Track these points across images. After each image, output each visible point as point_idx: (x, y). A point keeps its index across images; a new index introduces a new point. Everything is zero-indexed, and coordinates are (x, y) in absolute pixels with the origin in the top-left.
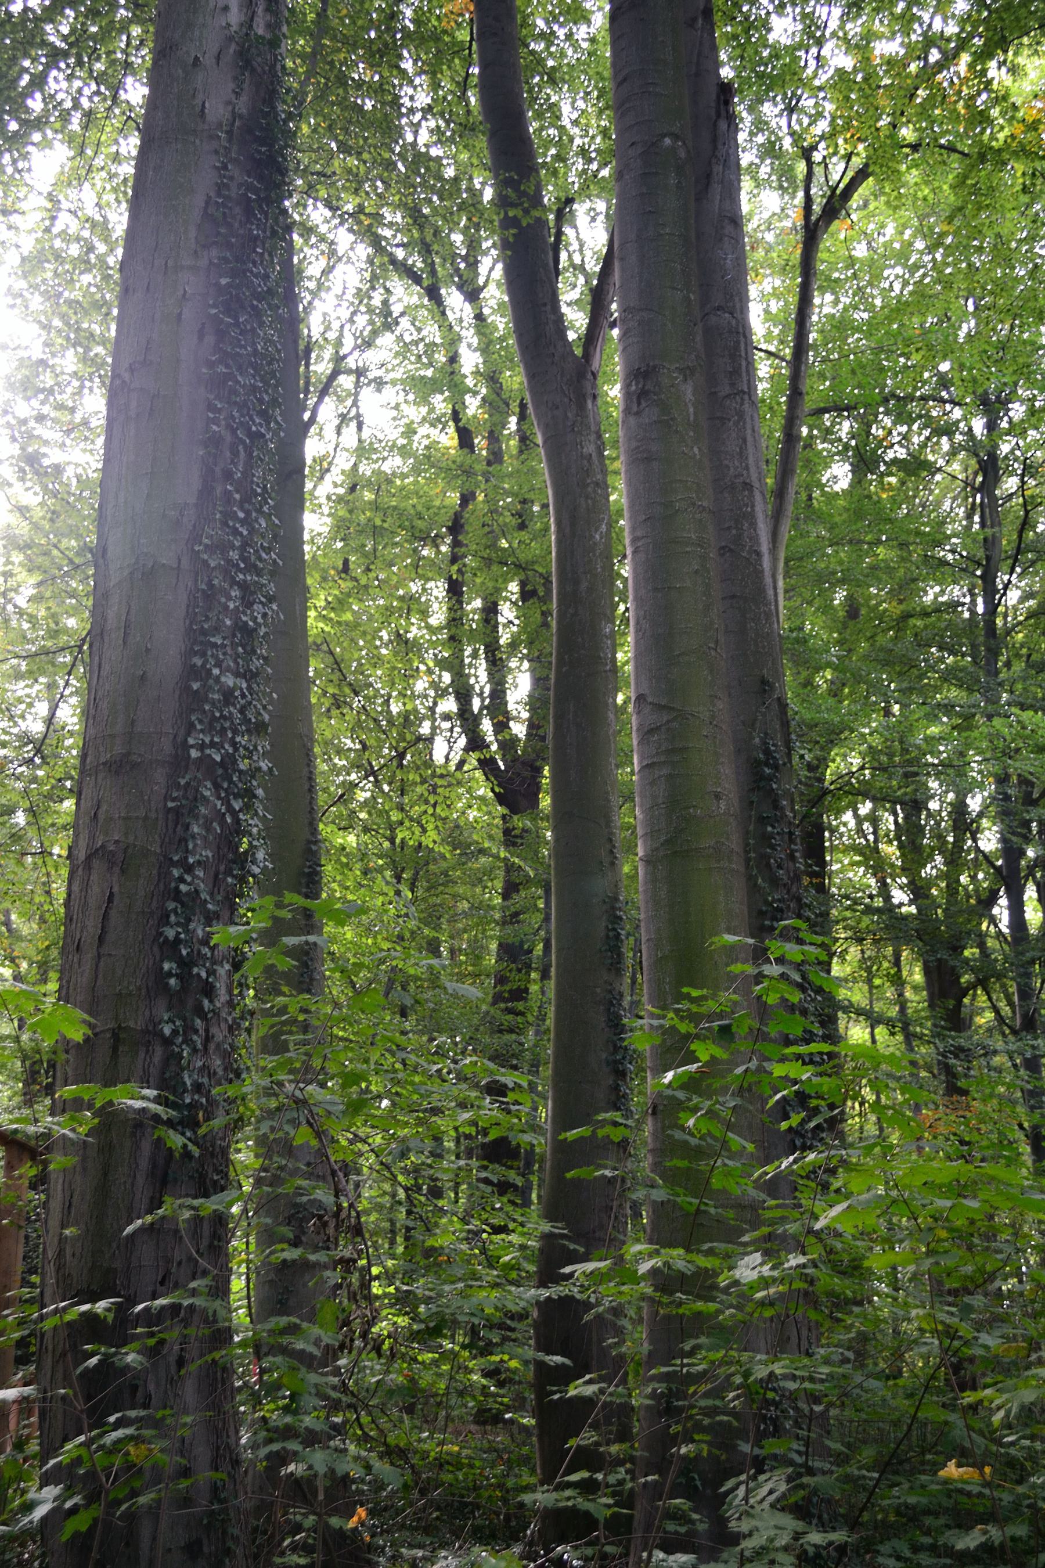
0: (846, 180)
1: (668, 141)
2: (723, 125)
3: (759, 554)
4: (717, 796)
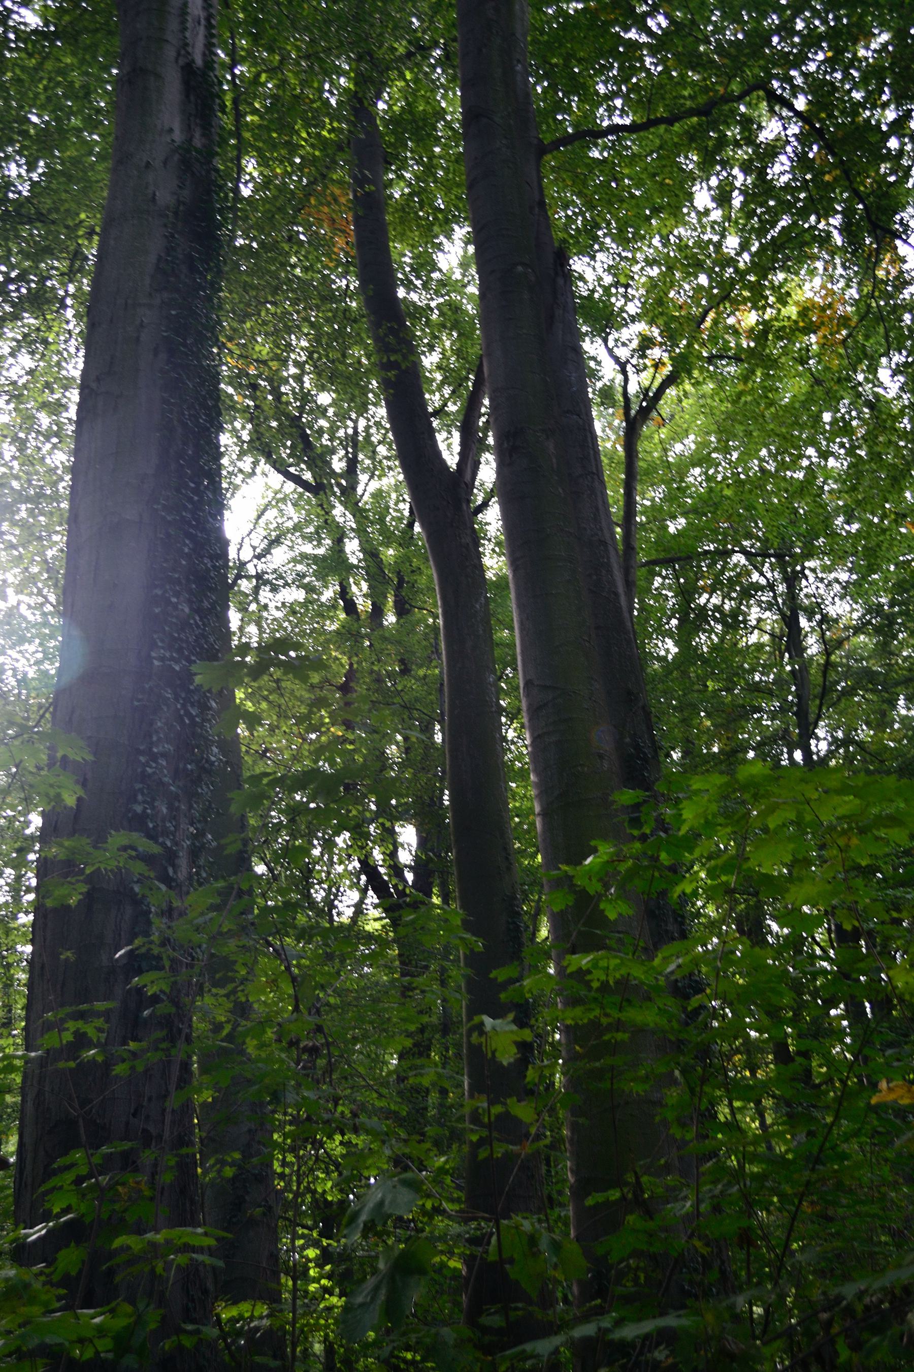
0: (656, 384)
1: (520, 269)
2: (560, 281)
3: (616, 594)
4: (601, 756)
